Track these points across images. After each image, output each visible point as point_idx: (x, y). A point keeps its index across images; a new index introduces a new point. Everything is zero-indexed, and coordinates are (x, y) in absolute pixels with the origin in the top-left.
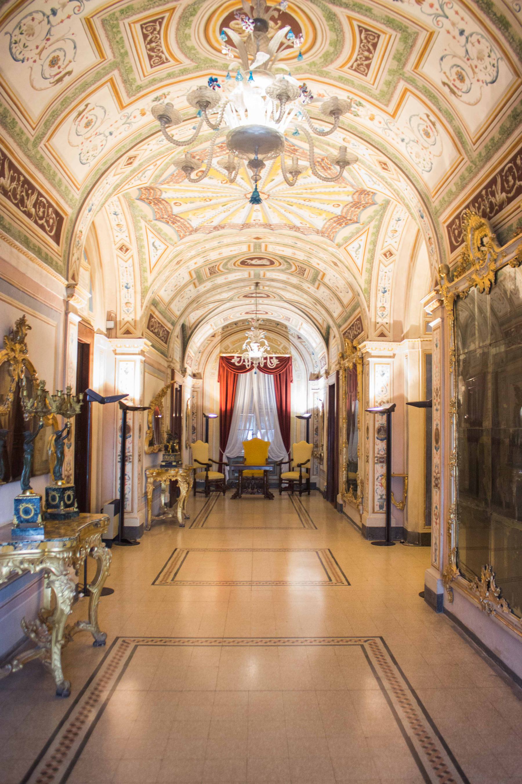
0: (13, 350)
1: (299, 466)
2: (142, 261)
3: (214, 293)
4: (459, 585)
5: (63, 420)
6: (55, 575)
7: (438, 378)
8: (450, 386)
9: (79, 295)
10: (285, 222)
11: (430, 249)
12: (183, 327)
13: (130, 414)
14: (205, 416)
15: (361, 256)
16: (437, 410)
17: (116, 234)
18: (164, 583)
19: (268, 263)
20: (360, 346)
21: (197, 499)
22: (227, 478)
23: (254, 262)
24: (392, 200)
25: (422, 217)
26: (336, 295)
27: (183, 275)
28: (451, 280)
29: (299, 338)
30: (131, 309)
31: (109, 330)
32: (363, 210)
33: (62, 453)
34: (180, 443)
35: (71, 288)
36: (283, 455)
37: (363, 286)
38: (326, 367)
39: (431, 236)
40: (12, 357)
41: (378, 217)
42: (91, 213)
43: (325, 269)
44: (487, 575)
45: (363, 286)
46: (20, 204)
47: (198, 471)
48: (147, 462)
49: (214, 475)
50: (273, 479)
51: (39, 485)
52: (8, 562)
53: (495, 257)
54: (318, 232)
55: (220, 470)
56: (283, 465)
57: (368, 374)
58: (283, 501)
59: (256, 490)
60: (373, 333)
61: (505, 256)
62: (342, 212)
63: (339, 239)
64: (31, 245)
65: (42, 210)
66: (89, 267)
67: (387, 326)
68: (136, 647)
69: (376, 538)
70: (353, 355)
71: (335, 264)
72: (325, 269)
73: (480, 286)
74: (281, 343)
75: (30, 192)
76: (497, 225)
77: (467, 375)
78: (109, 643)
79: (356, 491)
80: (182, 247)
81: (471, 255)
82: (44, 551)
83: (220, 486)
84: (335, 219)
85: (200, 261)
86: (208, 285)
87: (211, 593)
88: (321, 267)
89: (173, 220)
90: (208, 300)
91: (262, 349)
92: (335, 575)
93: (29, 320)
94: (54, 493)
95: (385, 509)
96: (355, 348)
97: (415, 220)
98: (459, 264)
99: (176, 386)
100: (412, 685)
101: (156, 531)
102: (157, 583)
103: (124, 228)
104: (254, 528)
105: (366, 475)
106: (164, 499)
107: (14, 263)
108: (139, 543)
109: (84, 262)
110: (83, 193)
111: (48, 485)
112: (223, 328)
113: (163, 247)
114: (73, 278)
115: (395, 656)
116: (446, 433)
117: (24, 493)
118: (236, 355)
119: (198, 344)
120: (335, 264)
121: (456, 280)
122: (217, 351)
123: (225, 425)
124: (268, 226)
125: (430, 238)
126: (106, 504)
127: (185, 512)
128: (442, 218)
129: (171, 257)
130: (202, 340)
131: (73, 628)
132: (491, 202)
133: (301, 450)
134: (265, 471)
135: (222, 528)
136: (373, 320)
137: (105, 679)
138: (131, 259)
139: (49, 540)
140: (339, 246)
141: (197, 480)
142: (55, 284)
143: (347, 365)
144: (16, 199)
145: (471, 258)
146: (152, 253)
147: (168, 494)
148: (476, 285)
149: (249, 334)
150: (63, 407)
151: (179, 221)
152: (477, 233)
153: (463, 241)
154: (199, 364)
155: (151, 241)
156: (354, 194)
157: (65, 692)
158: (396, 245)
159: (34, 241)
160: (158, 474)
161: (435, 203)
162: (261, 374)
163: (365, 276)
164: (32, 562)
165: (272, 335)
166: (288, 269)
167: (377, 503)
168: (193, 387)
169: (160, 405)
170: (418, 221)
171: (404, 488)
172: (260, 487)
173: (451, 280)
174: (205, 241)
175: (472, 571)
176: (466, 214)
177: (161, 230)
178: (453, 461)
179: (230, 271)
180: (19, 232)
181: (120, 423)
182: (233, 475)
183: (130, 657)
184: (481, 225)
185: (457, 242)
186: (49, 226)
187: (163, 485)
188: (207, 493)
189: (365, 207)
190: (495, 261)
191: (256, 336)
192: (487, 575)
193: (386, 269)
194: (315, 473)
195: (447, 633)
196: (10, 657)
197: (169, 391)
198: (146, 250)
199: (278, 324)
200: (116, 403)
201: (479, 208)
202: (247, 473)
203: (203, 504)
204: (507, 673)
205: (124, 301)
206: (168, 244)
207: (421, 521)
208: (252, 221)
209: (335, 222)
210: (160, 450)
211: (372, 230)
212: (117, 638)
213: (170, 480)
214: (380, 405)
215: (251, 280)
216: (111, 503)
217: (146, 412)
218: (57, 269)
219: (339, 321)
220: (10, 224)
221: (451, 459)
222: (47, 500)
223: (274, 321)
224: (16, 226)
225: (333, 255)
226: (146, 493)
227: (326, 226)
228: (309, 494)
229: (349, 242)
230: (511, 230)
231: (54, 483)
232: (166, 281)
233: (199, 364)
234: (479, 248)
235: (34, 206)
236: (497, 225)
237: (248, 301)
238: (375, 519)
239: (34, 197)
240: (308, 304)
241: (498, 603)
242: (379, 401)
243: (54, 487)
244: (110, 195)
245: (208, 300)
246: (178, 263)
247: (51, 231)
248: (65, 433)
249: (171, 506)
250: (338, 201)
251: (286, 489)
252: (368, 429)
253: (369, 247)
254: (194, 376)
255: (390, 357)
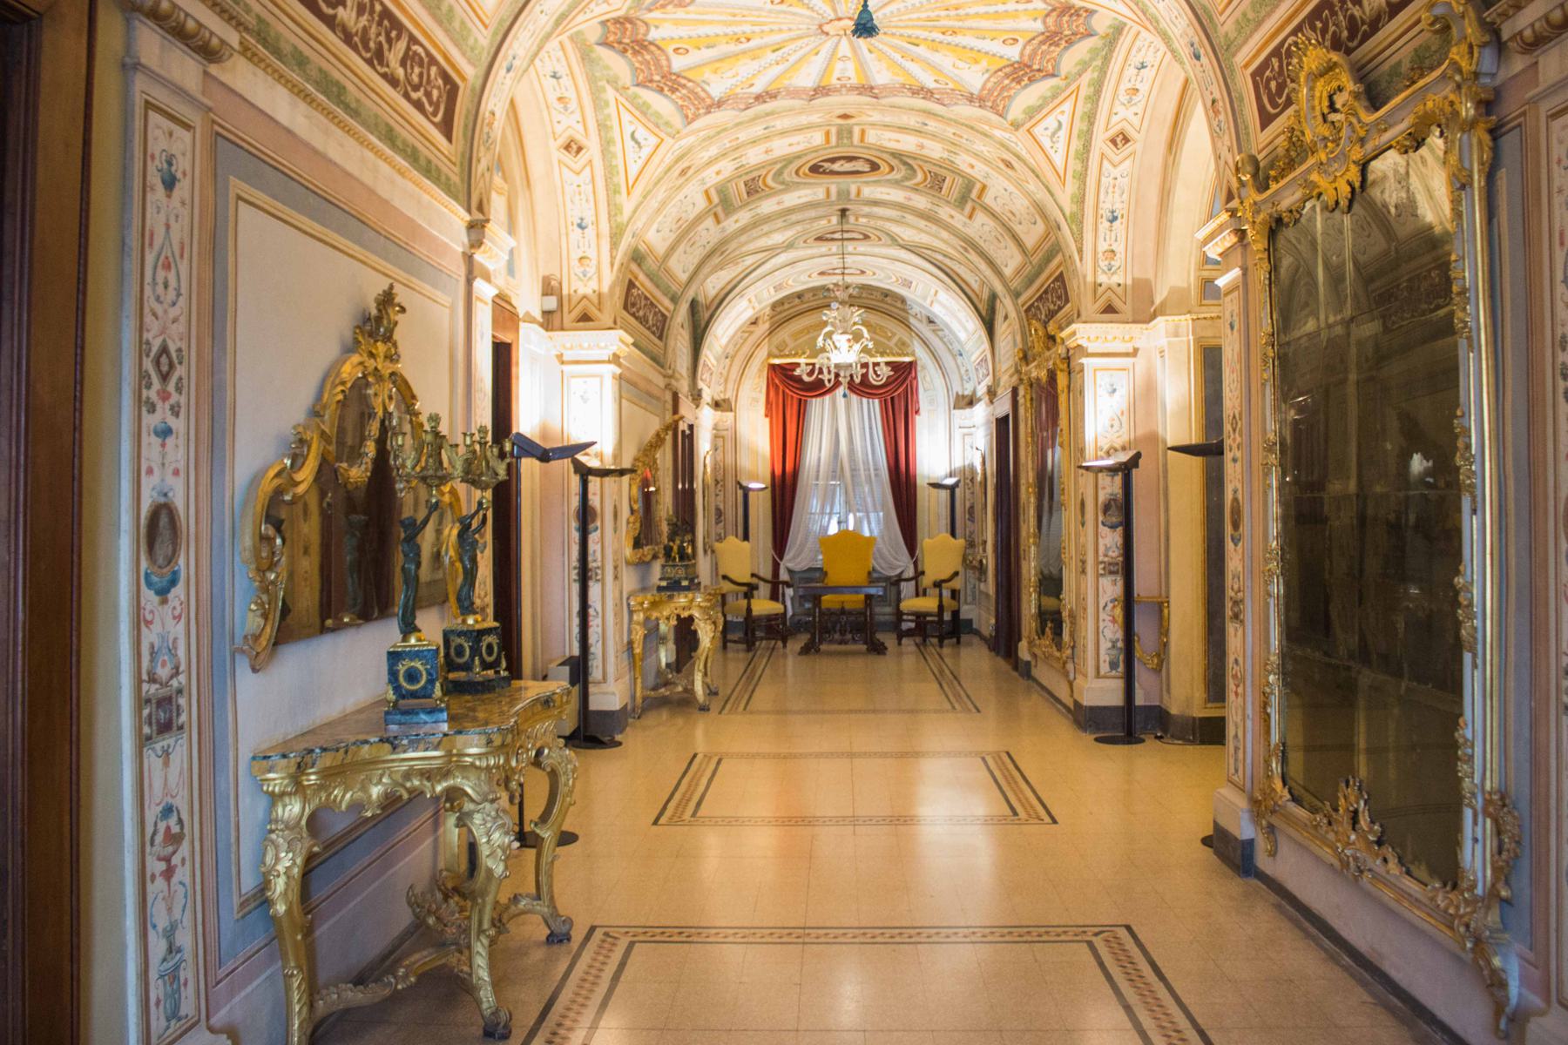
0: (372, 355)
1: (938, 585)
2: (610, 171)
3: (754, 233)
4: (1289, 819)
5: (469, 494)
6: (472, 800)
7: (1237, 393)
8: (1264, 408)
9: (492, 241)
10: (902, 80)
11: (1215, 123)
12: (694, 304)
13: (594, 483)
14: (742, 487)
15: (1061, 145)
16: (1235, 460)
17: (556, 116)
18: (676, 820)
19: (867, 168)
20: (1064, 334)
21: (730, 655)
22: (790, 613)
23: (836, 167)
24: (1130, 23)
25: (1197, 57)
26: (1010, 230)
27: (693, 198)
28: (1262, 186)
29: (931, 322)
30: (592, 270)
31: (546, 313)
32: (1066, 49)
33: (474, 560)
34: (693, 542)
35: (476, 228)
36: (904, 565)
37: (1069, 208)
38: (988, 381)
39: (1217, 95)
40: (371, 369)
41: (1098, 62)
42: (511, 74)
43: (987, 176)
44: (1352, 798)
45: (1069, 208)
46: (377, 58)
47: (730, 599)
48: (630, 580)
49: (763, 606)
50: (884, 612)
51: (432, 627)
52: (381, 776)
53: (1362, 133)
54: (971, 99)
55: (774, 596)
56: (903, 584)
57: (1082, 392)
58: (905, 656)
59: (849, 636)
60: (1089, 306)
61: (1385, 130)
62: (1022, 54)
63: (1016, 111)
64: (399, 143)
65: (417, 70)
66: (506, 187)
67: (1120, 291)
68: (632, 944)
69: (1105, 730)
70: (1047, 354)
71: (1009, 165)
72: (987, 176)
73: (1329, 197)
74: (894, 334)
75: (394, 34)
76: (1364, 66)
77: (1290, 390)
78: (577, 935)
79: (1060, 634)
80: (692, 139)
81: (1307, 132)
82: (449, 754)
83: (776, 629)
84: (1008, 70)
85: (727, 167)
86: (744, 217)
87: (761, 842)
88: (979, 171)
89: (671, 83)
90: (744, 249)
91: (857, 347)
92: (1019, 801)
93: (402, 295)
94: (461, 641)
95: (1121, 669)
96: (1052, 338)
97: (1182, 63)
98: (1281, 152)
99: (683, 426)
100: (1200, 1021)
101: (651, 719)
102: (663, 820)
103: (573, 105)
104: (851, 711)
105: (1081, 599)
106: (665, 655)
107: (367, 178)
108: (620, 744)
109: (498, 180)
110: (495, 34)
111: (446, 625)
112: (774, 306)
113: (653, 140)
114: (480, 208)
115: (1159, 964)
116: (1255, 506)
117: (405, 639)
118: (802, 360)
119: (724, 341)
120: (1009, 165)
121: (1274, 187)
122: (762, 354)
123: (783, 501)
124: (867, 89)
125: (1214, 102)
126: (553, 665)
127: (708, 680)
128: (1241, 58)
129: (669, 159)
130: (731, 332)
131: (507, 908)
132: (1352, 17)
133: (941, 553)
134: (869, 597)
135: (781, 712)
136: (1090, 278)
137: (575, 1007)
138: (588, 169)
139: (460, 732)
140: (1016, 126)
141: (729, 618)
142: (446, 221)
143: (1034, 374)
144: (367, 49)
145: (1308, 137)
146: (630, 156)
147: (671, 646)
148: (1320, 195)
149: (830, 315)
150: (474, 467)
151: (684, 86)
152: (1320, 84)
153: (1289, 103)
154: (726, 381)
155: (628, 130)
156: (1048, 15)
157: (500, 1030)
158: (1136, 121)
159: (404, 133)
160: (654, 605)
161: (1226, 25)
162: (854, 398)
163: (1071, 187)
164: (427, 775)
165: (874, 318)
166: (906, 178)
167: (1105, 658)
168: (715, 428)
169: (653, 465)
170: (1187, 66)
171: (1161, 625)
172: (859, 630)
173: (1262, 186)
174: (737, 125)
175: (1315, 792)
176: (1296, 44)
177: (649, 107)
178: (1273, 565)
179: (788, 187)
180: (376, 116)
181: (575, 502)
182: (801, 605)
183: (622, 965)
184: (1331, 67)
185: (1274, 105)
186: (431, 103)
187: (663, 628)
188: (749, 643)
189: (1070, 43)
190: (1362, 141)
191: (844, 320)
192: (1352, 798)
193: (1116, 172)
194: (969, 599)
195: (1264, 918)
196: (388, 963)
197: (669, 438)
198: (617, 149)
199: (886, 294)
200: (567, 462)
201: (1324, 31)
202: (829, 601)
203: (742, 667)
204: (1398, 997)
205: (575, 255)
206: (662, 135)
207: (1199, 693)
208: (834, 81)
209: (1007, 76)
210: (655, 557)
211: (1085, 91)
212: (593, 929)
213: (678, 616)
214: (1108, 454)
215: (831, 204)
216: (563, 664)
217: (626, 479)
218: (449, 189)
219: (1014, 285)
220: (358, 101)
221: (1267, 561)
222: (447, 655)
223: (877, 289)
224: (369, 105)
225: (1003, 145)
226: (630, 643)
227: (989, 85)
228: (958, 642)
229: (1038, 117)
230: (1399, 74)
231: (459, 620)
232: (659, 210)
233: (726, 381)
234: (1324, 116)
235: (403, 63)
236: (1364, 66)
237: (824, 248)
238: (1102, 691)
239: (401, 46)
240: (950, 250)
241: (1377, 855)
242: (1106, 448)
243: (460, 628)
244: (547, 37)
245: (744, 249)
246: (683, 172)
247: (435, 114)
248: (475, 524)
249: (679, 671)
250: (1015, 31)
251: (909, 633)
252: (1083, 504)
253: (1080, 125)
254: (717, 405)
255: (1127, 355)
